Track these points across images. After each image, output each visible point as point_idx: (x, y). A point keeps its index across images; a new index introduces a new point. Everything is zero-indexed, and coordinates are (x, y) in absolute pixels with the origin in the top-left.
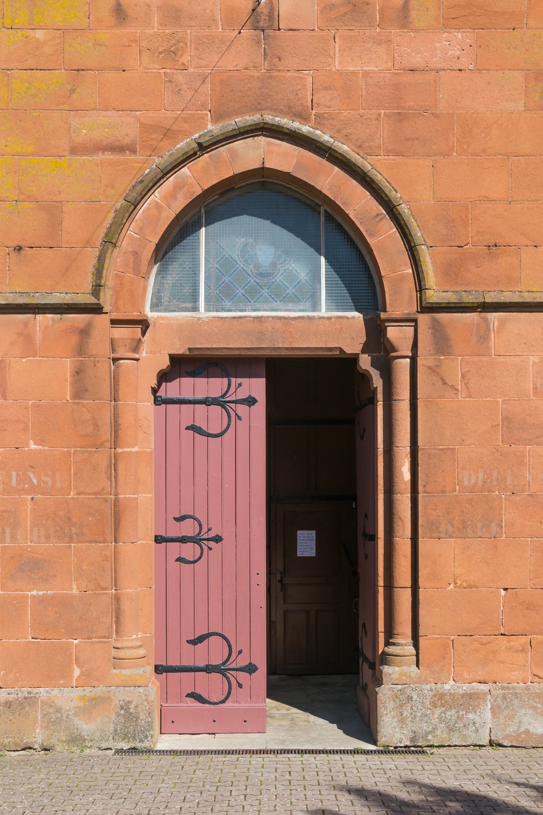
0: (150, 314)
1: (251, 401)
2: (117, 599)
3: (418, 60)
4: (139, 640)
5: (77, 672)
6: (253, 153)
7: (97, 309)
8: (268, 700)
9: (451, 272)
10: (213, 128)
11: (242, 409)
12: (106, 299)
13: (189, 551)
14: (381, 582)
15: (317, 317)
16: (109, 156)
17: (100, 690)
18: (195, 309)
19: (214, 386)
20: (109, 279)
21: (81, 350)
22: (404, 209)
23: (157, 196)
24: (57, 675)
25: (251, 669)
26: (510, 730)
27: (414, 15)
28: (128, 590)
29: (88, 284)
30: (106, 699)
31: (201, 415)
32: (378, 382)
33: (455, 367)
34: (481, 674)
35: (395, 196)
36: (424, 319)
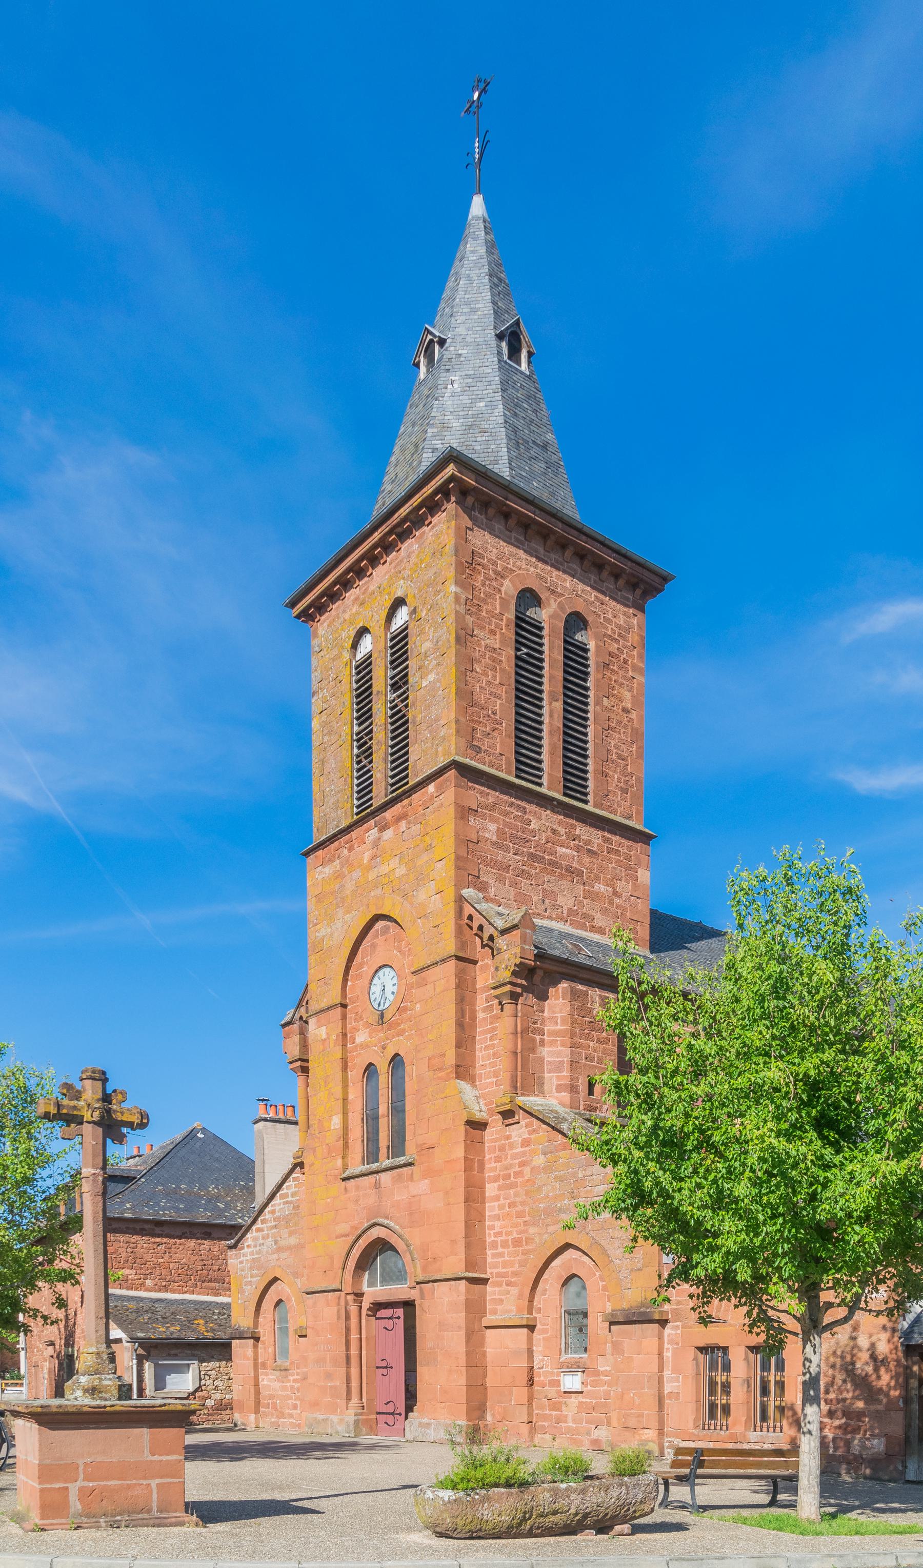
13: (384, 1371)
21: (338, 1304)
24: (334, 1412)
36: (418, 1286)
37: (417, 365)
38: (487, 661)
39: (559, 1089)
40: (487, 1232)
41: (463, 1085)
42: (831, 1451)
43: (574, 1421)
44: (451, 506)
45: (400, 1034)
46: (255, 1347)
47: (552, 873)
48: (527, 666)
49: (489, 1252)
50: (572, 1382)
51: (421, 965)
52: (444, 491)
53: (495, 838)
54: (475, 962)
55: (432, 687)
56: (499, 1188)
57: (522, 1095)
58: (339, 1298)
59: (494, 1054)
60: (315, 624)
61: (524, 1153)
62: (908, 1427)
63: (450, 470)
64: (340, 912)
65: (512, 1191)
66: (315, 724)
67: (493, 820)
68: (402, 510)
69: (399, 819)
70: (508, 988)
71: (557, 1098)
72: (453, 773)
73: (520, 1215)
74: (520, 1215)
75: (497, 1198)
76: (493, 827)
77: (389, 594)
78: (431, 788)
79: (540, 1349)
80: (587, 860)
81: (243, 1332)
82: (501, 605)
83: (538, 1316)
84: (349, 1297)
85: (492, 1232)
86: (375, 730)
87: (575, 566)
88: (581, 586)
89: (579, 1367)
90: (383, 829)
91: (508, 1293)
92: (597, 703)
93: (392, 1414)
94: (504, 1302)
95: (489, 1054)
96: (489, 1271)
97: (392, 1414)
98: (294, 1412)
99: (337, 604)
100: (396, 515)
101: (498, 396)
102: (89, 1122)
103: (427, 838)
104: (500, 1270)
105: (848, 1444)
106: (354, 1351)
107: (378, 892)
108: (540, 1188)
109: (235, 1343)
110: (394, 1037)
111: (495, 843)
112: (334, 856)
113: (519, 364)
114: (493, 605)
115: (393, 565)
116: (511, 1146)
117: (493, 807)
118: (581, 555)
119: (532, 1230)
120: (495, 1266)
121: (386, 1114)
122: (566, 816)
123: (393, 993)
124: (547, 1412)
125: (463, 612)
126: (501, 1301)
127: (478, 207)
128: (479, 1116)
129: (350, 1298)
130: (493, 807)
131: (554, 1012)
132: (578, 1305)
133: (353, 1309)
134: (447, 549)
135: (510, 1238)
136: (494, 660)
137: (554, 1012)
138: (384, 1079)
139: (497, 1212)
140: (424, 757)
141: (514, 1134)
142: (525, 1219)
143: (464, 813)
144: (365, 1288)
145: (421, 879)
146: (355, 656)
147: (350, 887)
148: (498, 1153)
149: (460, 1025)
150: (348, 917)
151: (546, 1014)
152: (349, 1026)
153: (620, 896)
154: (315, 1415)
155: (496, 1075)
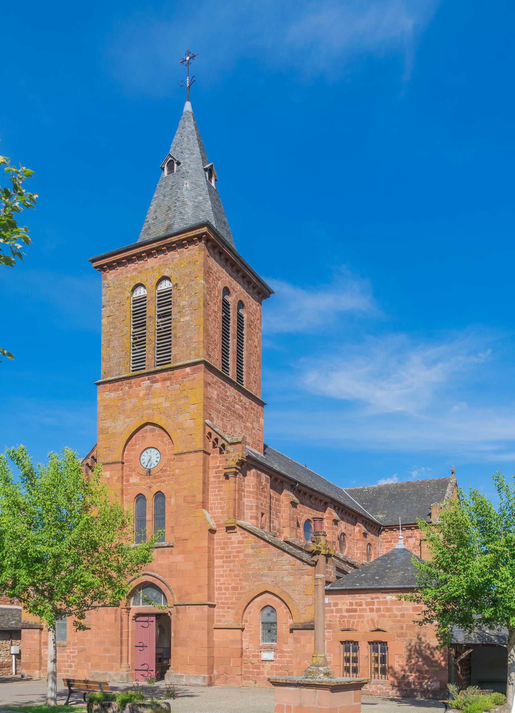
1: (152, 621)
3: (174, 560)
13: (141, 648)
19: (145, 618)
21: (116, 613)
24: (111, 669)
27: (173, 552)
30: (119, 674)
33: (180, 616)
36: (174, 607)
37: (163, 169)
38: (213, 316)
39: (251, 518)
40: (215, 582)
41: (205, 511)
42: (413, 687)
43: (268, 674)
44: (202, 244)
45: (163, 481)
46: (40, 633)
47: (234, 416)
48: (226, 320)
49: (216, 592)
50: (267, 656)
51: (180, 451)
52: (200, 237)
53: (216, 398)
54: (209, 454)
55: (188, 323)
56: (223, 562)
57: (238, 519)
58: (116, 610)
59: (221, 499)
60: (105, 273)
61: (240, 547)
63: (205, 229)
64: (122, 417)
65: (232, 564)
66: (104, 321)
67: (216, 390)
68: (173, 238)
69: (165, 380)
70: (234, 470)
71: (250, 522)
72: (203, 365)
73: (236, 576)
74: (236, 576)
75: (222, 567)
76: (215, 392)
77: (159, 273)
78: (188, 370)
79: (247, 640)
80: (244, 411)
81: (33, 625)
82: (218, 292)
83: (246, 624)
84: (123, 610)
85: (218, 583)
86: (148, 333)
87: (241, 280)
88: (242, 289)
89: (271, 649)
90: (154, 382)
91: (229, 612)
92: (247, 342)
93: (147, 670)
94: (225, 616)
95: (217, 498)
96: (216, 601)
97: (147, 670)
98: (70, 669)
99: (121, 268)
100: (169, 239)
101: (208, 197)
102: (322, 554)
103: (184, 392)
104: (223, 601)
105: (420, 684)
106: (125, 638)
107: (150, 411)
108: (250, 564)
109: (23, 631)
110: (157, 483)
111: (216, 400)
112: (118, 389)
113: (211, 182)
114: (215, 292)
115: (162, 260)
116: (232, 543)
117: (215, 384)
118: (244, 277)
119: (244, 583)
120: (221, 599)
121: (151, 520)
122: (239, 391)
123: (157, 461)
124: (251, 670)
125: (206, 293)
126: (224, 616)
127: (188, 106)
128: (214, 527)
129: (124, 610)
130: (215, 384)
131: (249, 482)
132: (271, 619)
133: (125, 616)
134: (198, 263)
135: (230, 586)
136: (215, 317)
137: (249, 482)
138: (150, 503)
139: (222, 573)
140: (180, 354)
141: (233, 537)
142: (240, 578)
143: (207, 384)
144: (131, 606)
145: (180, 411)
146: (132, 295)
147: (129, 406)
148: (222, 545)
149: (204, 483)
150: (127, 420)
151: (245, 483)
152: (124, 473)
153: (254, 429)
155: (221, 508)
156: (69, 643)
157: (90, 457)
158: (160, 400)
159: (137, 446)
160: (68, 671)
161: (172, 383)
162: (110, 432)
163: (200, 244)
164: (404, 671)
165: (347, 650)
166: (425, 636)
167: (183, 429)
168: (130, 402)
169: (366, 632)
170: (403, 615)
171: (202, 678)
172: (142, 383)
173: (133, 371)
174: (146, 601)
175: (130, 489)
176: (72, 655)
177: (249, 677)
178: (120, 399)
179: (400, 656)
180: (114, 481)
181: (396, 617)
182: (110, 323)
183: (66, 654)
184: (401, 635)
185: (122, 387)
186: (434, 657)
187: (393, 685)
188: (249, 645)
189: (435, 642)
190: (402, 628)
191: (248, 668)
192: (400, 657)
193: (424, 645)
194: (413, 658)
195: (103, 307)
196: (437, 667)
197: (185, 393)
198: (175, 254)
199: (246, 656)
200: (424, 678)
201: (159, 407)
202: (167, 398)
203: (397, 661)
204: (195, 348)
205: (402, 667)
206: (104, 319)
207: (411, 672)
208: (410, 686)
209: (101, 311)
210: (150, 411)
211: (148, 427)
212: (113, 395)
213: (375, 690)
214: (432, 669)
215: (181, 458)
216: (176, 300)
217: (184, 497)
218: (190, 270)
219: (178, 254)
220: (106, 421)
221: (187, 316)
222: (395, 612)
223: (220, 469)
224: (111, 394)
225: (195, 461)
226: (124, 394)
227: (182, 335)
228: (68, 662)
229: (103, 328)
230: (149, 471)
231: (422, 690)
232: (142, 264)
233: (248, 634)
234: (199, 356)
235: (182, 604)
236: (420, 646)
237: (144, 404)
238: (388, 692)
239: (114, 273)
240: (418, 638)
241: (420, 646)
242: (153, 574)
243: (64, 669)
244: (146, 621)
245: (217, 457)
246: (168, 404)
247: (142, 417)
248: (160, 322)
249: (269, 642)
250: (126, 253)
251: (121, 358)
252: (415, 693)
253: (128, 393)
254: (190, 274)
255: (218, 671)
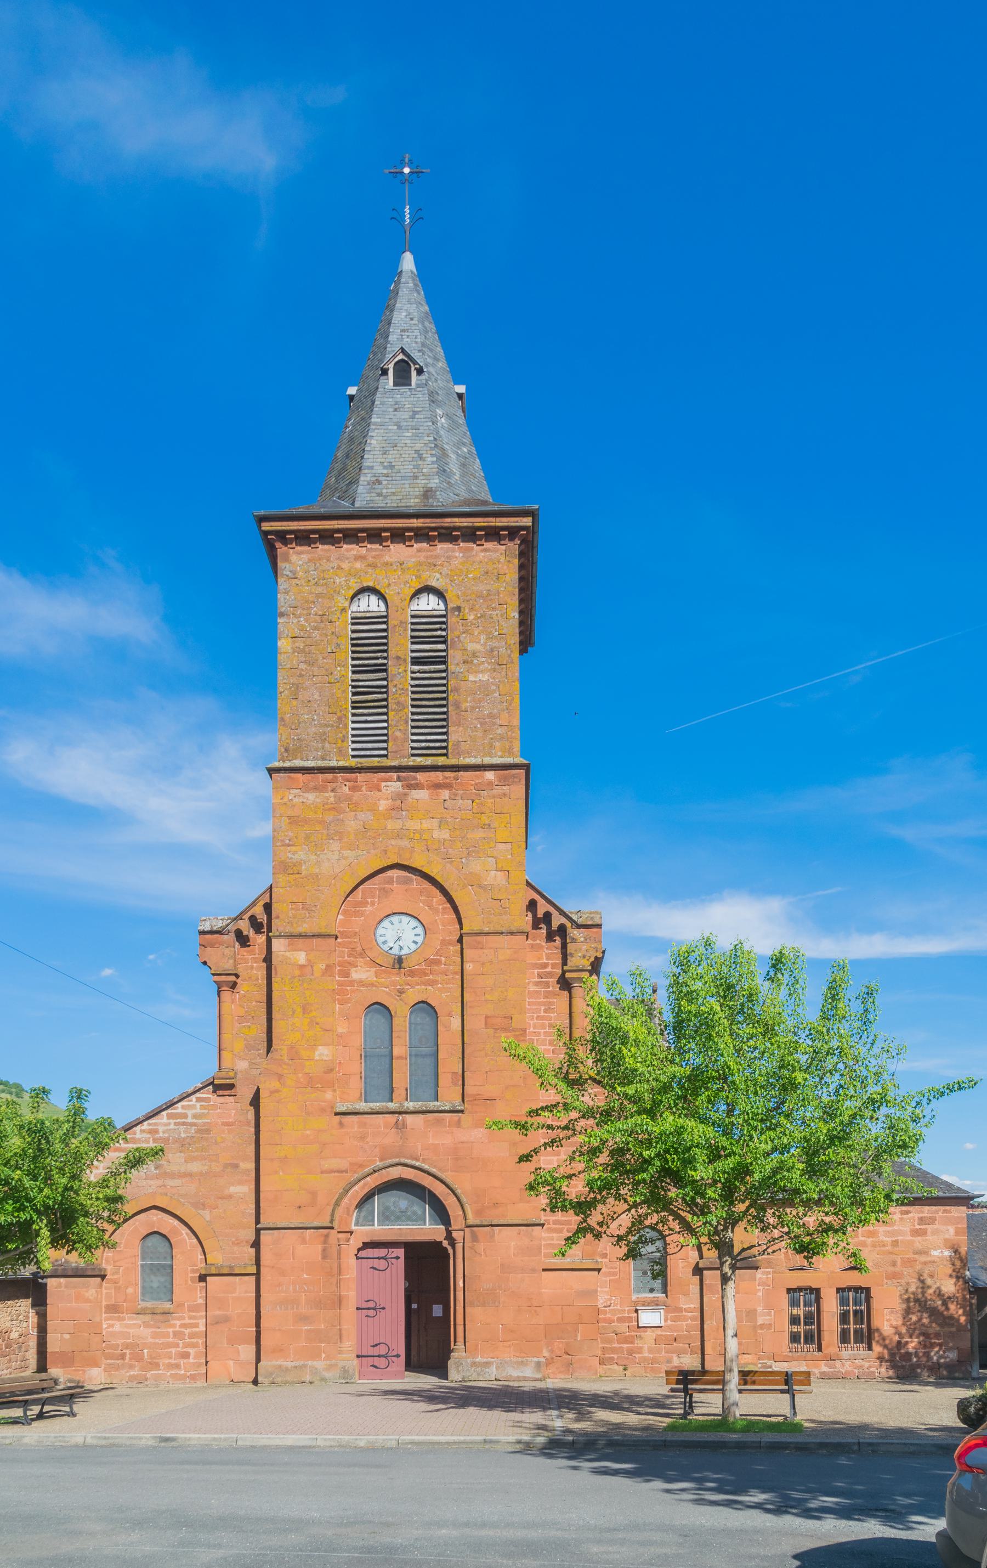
0: (353, 1228)
1: (398, 1258)
2: (340, 1330)
3: (464, 1139)
4: (350, 1344)
5: (323, 1355)
6: (395, 1173)
7: (332, 1228)
8: (407, 1373)
9: (478, 1213)
10: (379, 1164)
11: (394, 1261)
12: (335, 1224)
13: (371, 1313)
14: (452, 1323)
15: (427, 1229)
16: (337, 1174)
17: (334, 1362)
18: (373, 1225)
19: (382, 1252)
20: (337, 1217)
21: (325, 1242)
22: (459, 1192)
23: (356, 1188)
24: (316, 1356)
25: (398, 1356)
26: (504, 1375)
27: (462, 1123)
28: (344, 1327)
29: (328, 1218)
31: (376, 1263)
32: (450, 1251)
33: (480, 1247)
34: (491, 1355)
35: (454, 1186)
36: (467, 1229)
37: (385, 372)
43: (650, 1351)
45: (432, 983)
50: (649, 1318)
52: (513, 532)
55: (484, 688)
62: (972, 1341)
64: (335, 845)
66: (284, 644)
68: (456, 520)
69: (437, 786)
77: (418, 577)
78: (490, 775)
89: (657, 1305)
90: (410, 787)
93: (385, 1356)
97: (385, 1356)
99: (326, 547)
100: (449, 520)
105: (927, 1355)
107: (405, 843)
110: (418, 984)
123: (415, 942)
124: (616, 1345)
127: (408, 262)
134: (508, 578)
140: (466, 741)
150: (347, 853)
154: (278, 1363)
156: (181, 1305)
157: (246, 917)
158: (426, 824)
159: (369, 908)
160: (177, 1366)
161: (455, 795)
162: (304, 873)
163: (511, 544)
164: (900, 1335)
165: (794, 1303)
166: (932, 1276)
167: (480, 886)
168: (356, 818)
169: (834, 1272)
170: (895, 1243)
171: (533, 1365)
172: (384, 784)
173: (353, 756)
174: (386, 1217)
175: (353, 991)
176: (187, 1331)
177: (612, 1359)
178: (329, 809)
179: (892, 1311)
180: (317, 973)
181: (884, 1246)
182: (296, 650)
183: (171, 1330)
184: (894, 1276)
185: (334, 785)
186: (947, 1309)
187: (881, 1359)
188: (610, 1300)
189: (949, 1287)
190: (894, 1264)
191: (610, 1341)
192: (892, 1312)
193: (931, 1291)
194: (913, 1313)
195: (282, 615)
196: (953, 1325)
197: (484, 819)
198: (454, 551)
199: (605, 1320)
200: (932, 1346)
201: (425, 837)
202: (442, 823)
203: (888, 1318)
204: (502, 738)
205: (896, 1328)
206: (283, 640)
207: (911, 1337)
208: (910, 1360)
209: (277, 624)
210: (405, 843)
211: (395, 873)
212: (311, 797)
213: (850, 1369)
214: (946, 1329)
215: (479, 943)
216: (458, 637)
217: (487, 1017)
218: (488, 587)
219: (461, 550)
220: (294, 848)
221: (482, 672)
222: (882, 1238)
223: (549, 969)
224: (306, 795)
225: (508, 952)
226: (339, 800)
227: (473, 708)
228: (177, 1346)
229: (281, 658)
230: (400, 960)
231: (930, 1363)
232: (376, 550)
233: (608, 1279)
234: (510, 753)
235: (486, 1223)
236: (923, 1293)
237: (389, 827)
238: (873, 1372)
239: (308, 552)
240: (919, 1279)
241: (923, 1293)
242: (417, 1164)
243: (167, 1361)
244: (382, 1258)
245: (541, 947)
246: (445, 835)
247: (386, 852)
248: (419, 672)
249: (645, 1292)
250: (346, 522)
251: (326, 726)
252: (919, 1371)
253: (348, 799)
254: (489, 595)
255: (552, 1351)
